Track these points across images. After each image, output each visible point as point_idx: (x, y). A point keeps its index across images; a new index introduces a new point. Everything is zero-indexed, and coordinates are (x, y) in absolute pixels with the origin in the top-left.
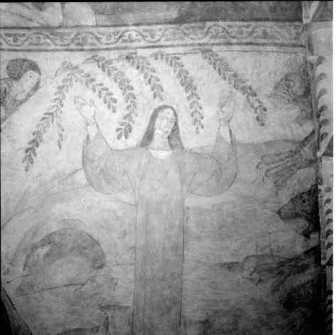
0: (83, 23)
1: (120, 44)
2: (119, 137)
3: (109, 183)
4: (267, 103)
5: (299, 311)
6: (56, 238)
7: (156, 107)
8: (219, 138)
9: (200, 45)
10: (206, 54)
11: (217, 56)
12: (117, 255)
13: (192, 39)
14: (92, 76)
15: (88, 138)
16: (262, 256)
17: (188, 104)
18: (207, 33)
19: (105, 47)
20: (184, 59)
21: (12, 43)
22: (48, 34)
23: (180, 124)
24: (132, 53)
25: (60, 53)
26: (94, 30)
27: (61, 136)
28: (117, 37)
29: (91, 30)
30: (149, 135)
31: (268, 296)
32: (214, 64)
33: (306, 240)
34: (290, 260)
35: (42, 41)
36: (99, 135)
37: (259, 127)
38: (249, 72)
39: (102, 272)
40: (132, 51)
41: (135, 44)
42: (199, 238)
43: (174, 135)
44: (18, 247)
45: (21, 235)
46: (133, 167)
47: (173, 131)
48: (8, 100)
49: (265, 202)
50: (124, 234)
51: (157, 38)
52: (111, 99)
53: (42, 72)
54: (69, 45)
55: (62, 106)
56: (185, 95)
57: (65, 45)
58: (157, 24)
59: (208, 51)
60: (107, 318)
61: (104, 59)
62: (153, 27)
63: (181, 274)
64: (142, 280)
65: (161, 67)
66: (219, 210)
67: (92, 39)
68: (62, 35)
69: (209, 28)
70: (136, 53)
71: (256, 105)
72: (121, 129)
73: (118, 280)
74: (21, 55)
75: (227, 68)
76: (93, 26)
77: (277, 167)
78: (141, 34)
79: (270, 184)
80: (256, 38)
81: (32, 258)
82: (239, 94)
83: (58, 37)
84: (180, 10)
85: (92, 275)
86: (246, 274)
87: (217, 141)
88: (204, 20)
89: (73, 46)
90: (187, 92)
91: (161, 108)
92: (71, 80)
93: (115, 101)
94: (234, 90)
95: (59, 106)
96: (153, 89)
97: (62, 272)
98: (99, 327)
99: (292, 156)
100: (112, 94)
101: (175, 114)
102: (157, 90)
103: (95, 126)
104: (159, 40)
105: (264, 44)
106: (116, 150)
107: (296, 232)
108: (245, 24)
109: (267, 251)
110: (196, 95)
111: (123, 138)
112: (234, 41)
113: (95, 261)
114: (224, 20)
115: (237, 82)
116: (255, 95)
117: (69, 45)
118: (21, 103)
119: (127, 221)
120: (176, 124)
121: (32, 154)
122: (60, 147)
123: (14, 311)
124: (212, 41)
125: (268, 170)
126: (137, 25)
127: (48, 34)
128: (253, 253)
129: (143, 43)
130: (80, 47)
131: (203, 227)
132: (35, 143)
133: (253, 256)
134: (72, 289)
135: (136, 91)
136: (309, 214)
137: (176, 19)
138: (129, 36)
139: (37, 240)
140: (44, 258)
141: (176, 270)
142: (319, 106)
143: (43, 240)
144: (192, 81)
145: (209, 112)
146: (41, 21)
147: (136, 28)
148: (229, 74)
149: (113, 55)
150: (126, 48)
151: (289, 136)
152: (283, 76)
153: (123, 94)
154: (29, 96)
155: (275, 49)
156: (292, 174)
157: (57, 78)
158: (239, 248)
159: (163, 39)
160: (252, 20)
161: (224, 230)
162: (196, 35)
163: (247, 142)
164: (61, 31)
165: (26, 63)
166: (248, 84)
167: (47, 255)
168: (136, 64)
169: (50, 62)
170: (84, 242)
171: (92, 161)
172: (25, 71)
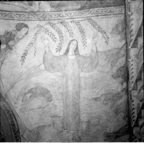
0: (46, 10)
1: (59, 18)
2: (57, 52)
3: (53, 69)
4: (110, 36)
5: (120, 114)
6: (34, 90)
7: (70, 40)
8: (92, 50)
9: (87, 17)
10: (89, 20)
11: (93, 20)
12: (56, 96)
13: (85, 15)
14: (48, 29)
15: (45, 52)
16: (107, 94)
17: (82, 38)
18: (90, 13)
19: (53, 19)
20: (81, 23)
21: (18, 17)
22: (32, 14)
23: (79, 46)
24: (63, 21)
25: (36, 21)
26: (50, 13)
27: (35, 51)
28: (58, 15)
29: (49, 13)
30: (67, 51)
31: (109, 110)
32: (92, 24)
33: (122, 86)
34: (117, 94)
35: (30, 17)
36: (50, 51)
37: (107, 45)
38: (104, 25)
39: (51, 103)
40: (62, 20)
41: (64, 18)
42: (85, 89)
43: (77, 49)
44: (19, 94)
45: (20, 90)
46: (62, 63)
47: (76, 49)
48: (15, 38)
49: (108, 73)
50: (59, 88)
51: (72, 15)
52: (55, 37)
53: (29, 28)
54: (40, 18)
55: (36, 40)
56: (81, 35)
57: (39, 18)
58: (73, 10)
59: (90, 19)
60: (54, 121)
61: (52, 23)
62: (71, 12)
63: (79, 103)
64: (66, 106)
65: (72, 25)
66: (92, 78)
67: (49, 16)
68: (38, 15)
69: (91, 11)
70: (64, 21)
71: (106, 37)
72: (58, 49)
73: (57, 106)
74: (21, 22)
75: (96, 24)
76: (50, 12)
77: (112, 59)
78: (67, 14)
79: (109, 65)
80: (107, 13)
81: (25, 98)
82: (100, 34)
83: (36, 16)
84: (81, 5)
85: (48, 104)
86: (102, 101)
87: (91, 51)
88: (90, 8)
89: (41, 19)
90: (81, 34)
91: (72, 40)
92: (40, 31)
93: (56, 38)
94: (98, 32)
95: (35, 40)
96: (69, 34)
97: (36, 103)
98: (51, 124)
99: (117, 54)
100: (55, 36)
101: (77, 43)
102: (71, 34)
103: (48, 48)
104: (73, 16)
105: (110, 15)
106: (56, 56)
107: (119, 83)
108: (104, 8)
109: (109, 91)
110: (85, 35)
111: (58, 52)
112: (100, 15)
113: (48, 98)
114: (97, 7)
115: (100, 29)
116: (106, 33)
117: (40, 18)
118: (20, 39)
119: (60, 83)
120: (77, 46)
121: (24, 58)
122: (35, 55)
123: (19, 119)
124: (92, 15)
125: (109, 60)
126: (65, 11)
127: (32, 14)
128: (104, 93)
129: (67, 17)
130: (44, 19)
131: (86, 84)
132: (25, 54)
133: (104, 94)
134: (40, 110)
135: (64, 34)
136: (122, 75)
137: (80, 9)
138: (62, 15)
139: (26, 91)
140: (29, 98)
141: (77, 102)
142: (131, 30)
143: (28, 91)
144: (83, 30)
145: (89, 41)
146: (30, 10)
147: (65, 12)
148: (97, 26)
149: (56, 22)
150: (61, 19)
151: (117, 47)
152: (116, 25)
153: (59, 36)
154: (23, 37)
155: (113, 16)
156: (117, 61)
157: (35, 30)
158: (100, 92)
159: (75, 15)
160: (106, 7)
161: (93, 86)
162: (86, 13)
163: (102, 51)
164: (38, 13)
165: (23, 25)
166: (104, 29)
167: (31, 96)
168: (64, 25)
169: (32, 24)
170: (44, 91)
171: (47, 61)
172: (23, 27)
